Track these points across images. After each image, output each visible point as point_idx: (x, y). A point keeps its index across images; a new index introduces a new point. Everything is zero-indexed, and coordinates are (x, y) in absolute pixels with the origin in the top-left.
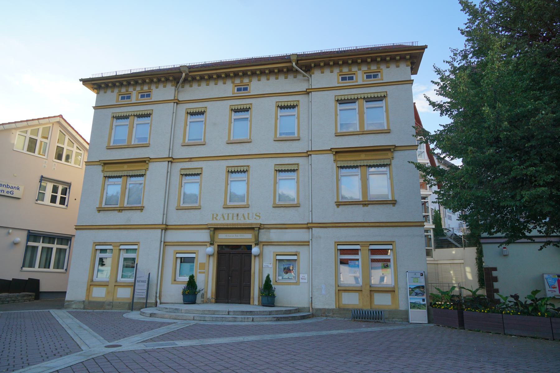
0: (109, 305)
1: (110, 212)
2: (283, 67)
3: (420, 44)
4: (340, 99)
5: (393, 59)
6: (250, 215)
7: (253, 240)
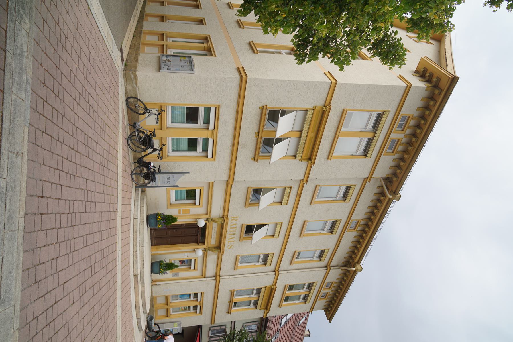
5: (427, 107)
6: (232, 242)
7: (209, 246)
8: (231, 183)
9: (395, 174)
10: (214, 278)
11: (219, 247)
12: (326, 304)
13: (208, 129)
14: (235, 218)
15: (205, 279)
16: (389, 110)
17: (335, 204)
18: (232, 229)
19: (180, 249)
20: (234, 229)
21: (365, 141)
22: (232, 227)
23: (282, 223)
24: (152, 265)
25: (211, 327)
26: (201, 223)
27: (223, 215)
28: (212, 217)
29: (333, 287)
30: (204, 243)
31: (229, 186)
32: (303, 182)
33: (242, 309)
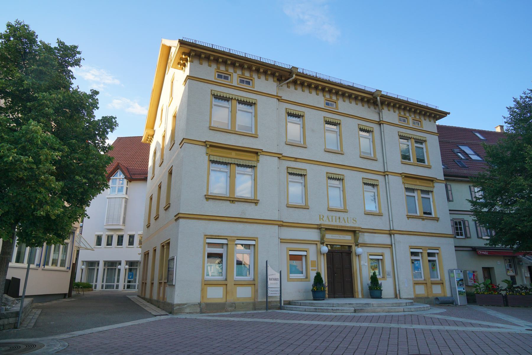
0: (231, 306)
1: (221, 201)
2: (365, 97)
3: (440, 108)
4: (216, 94)
5: (208, 58)
6: (349, 220)
7: (353, 241)
8: (281, 223)
9: (273, 75)
10: (392, 236)
11: (354, 232)
12: (427, 120)
13: (227, 244)
14: (321, 218)
15: (393, 245)
16: (210, 90)
17: (306, 125)
18: (334, 220)
19: (356, 271)
20: (334, 218)
21: (240, 107)
22: (331, 220)
23: (327, 173)
24: (373, 297)
25: (478, 237)
26: (325, 249)
27: (317, 228)
28: (319, 240)
29: (405, 114)
30: (350, 247)
31: (284, 224)
32: (280, 157)
33: (434, 206)
